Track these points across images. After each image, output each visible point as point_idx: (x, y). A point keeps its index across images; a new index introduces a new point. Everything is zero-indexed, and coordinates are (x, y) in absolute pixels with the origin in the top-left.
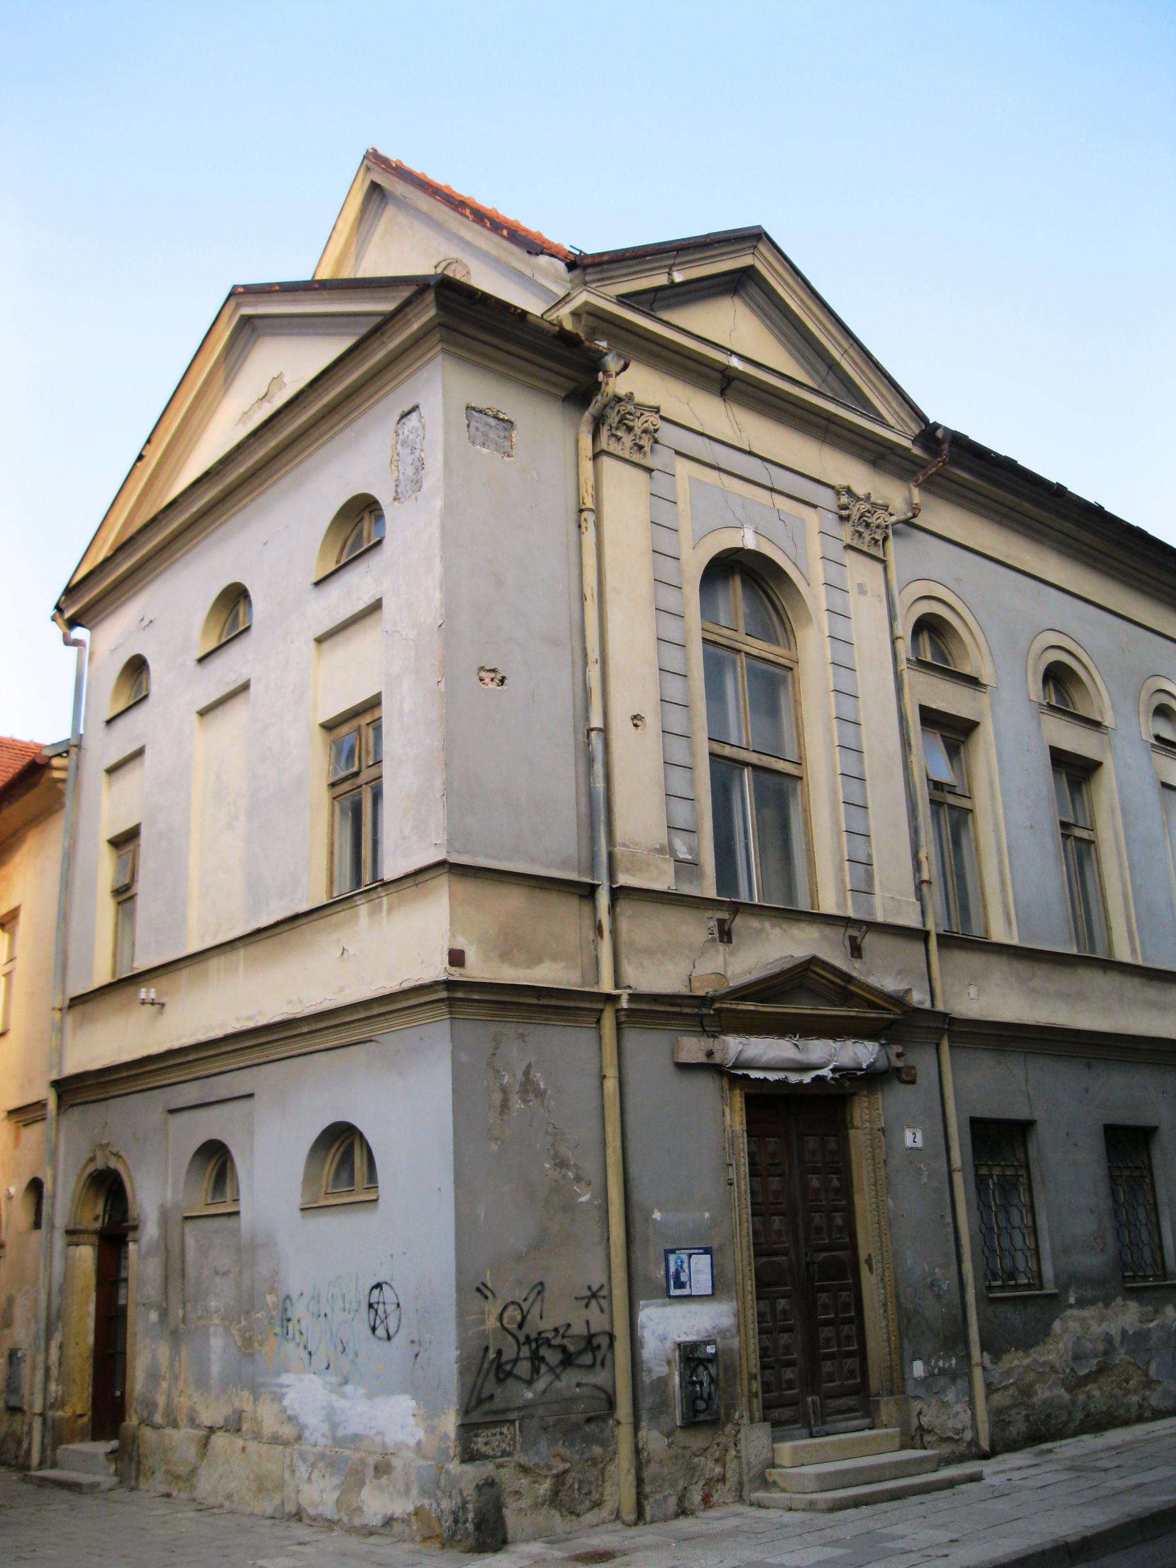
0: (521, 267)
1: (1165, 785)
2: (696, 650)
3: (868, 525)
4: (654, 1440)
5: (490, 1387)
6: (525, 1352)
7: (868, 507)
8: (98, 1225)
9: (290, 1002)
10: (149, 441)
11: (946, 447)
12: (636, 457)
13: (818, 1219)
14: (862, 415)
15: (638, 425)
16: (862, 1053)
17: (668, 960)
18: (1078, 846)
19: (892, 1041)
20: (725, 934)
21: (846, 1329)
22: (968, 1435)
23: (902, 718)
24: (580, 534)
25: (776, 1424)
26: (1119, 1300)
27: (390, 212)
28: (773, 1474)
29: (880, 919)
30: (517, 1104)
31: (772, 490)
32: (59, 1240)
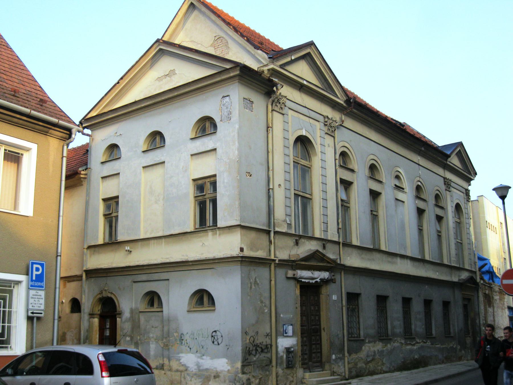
0: (253, 52)
1: (397, 199)
2: (292, 164)
3: (331, 127)
4: (280, 371)
5: (247, 356)
6: (254, 348)
7: (332, 121)
8: (99, 312)
9: (183, 255)
10: (122, 78)
11: (353, 104)
12: (281, 111)
13: (313, 318)
14: (333, 95)
15: (281, 101)
16: (325, 275)
17: (285, 251)
18: (374, 216)
19: (332, 272)
20: (297, 243)
21: (318, 346)
22: (343, 374)
23: (336, 182)
24: (268, 134)
25: (304, 369)
26: (377, 342)
27: (196, 13)
28: (305, 381)
29: (329, 239)
30: (253, 287)
31: (309, 117)
32: (85, 317)
